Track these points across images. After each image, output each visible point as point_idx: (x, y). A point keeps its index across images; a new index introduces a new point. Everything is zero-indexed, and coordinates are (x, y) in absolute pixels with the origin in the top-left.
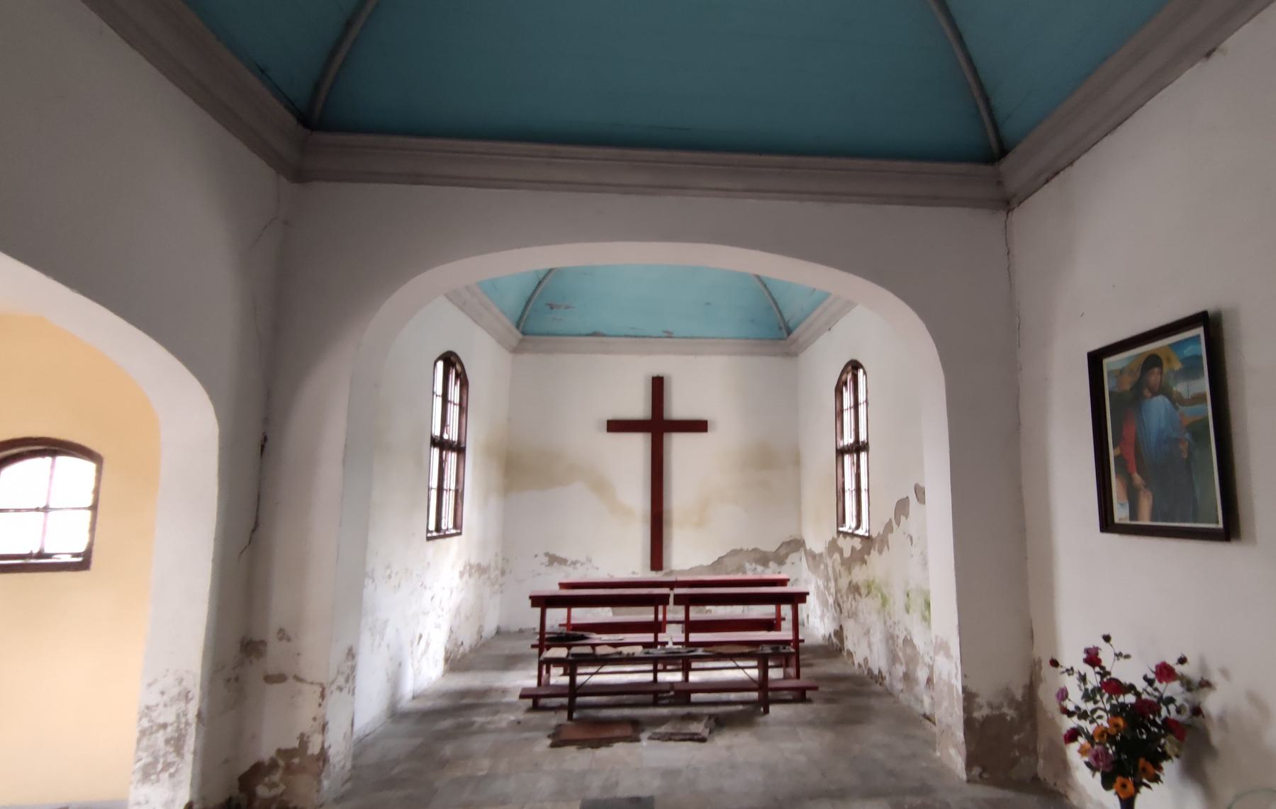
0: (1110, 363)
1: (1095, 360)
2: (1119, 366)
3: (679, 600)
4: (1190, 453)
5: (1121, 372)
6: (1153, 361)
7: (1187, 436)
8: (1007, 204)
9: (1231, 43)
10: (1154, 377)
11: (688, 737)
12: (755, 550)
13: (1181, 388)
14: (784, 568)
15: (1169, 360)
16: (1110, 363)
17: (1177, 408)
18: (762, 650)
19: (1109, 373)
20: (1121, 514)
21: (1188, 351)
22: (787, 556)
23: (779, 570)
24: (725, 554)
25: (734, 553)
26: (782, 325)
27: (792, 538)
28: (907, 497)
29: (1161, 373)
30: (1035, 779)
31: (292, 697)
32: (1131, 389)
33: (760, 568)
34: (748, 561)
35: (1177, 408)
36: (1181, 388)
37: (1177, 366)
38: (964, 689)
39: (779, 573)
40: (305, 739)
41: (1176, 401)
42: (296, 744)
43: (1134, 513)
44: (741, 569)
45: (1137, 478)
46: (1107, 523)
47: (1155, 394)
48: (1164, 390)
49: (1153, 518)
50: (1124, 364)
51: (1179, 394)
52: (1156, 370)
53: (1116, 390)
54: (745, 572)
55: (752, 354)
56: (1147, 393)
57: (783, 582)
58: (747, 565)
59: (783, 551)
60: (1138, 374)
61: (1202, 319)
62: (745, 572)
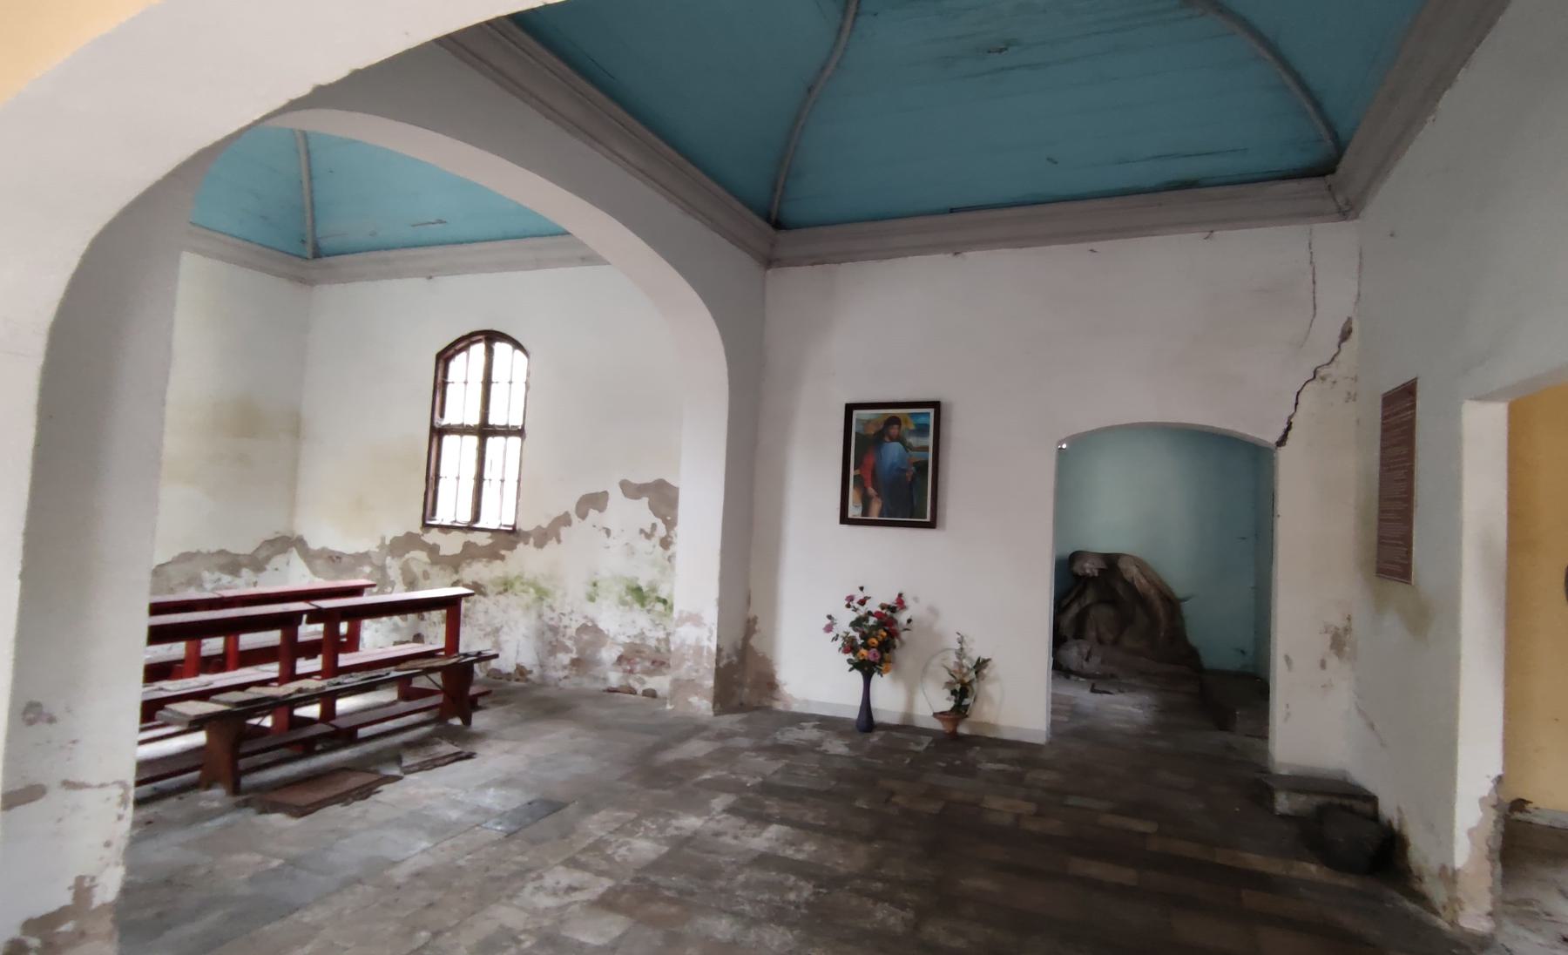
0: (856, 413)
1: (850, 408)
2: (867, 418)
3: (315, 616)
4: (913, 479)
5: (869, 422)
6: (894, 420)
7: (913, 468)
8: (769, 262)
9: (971, 255)
10: (894, 430)
11: (454, 758)
12: (222, 552)
13: (913, 441)
14: (264, 576)
15: (906, 422)
16: (856, 413)
17: (907, 451)
18: (695, 620)
19: (857, 420)
20: (854, 511)
21: (922, 420)
22: (268, 559)
23: (254, 580)
24: (170, 559)
25: (187, 557)
26: (310, 241)
27: (278, 536)
28: (606, 493)
29: (899, 428)
30: (742, 704)
31: (60, 820)
32: (874, 435)
33: (226, 579)
34: (208, 570)
35: (907, 451)
36: (913, 441)
37: (912, 427)
38: (718, 646)
39: (255, 584)
40: (87, 884)
41: (907, 447)
42: (66, 899)
43: (865, 511)
44: (195, 581)
45: (871, 491)
46: (845, 519)
47: (892, 440)
48: (900, 439)
49: (863, 516)
50: (873, 417)
51: (910, 444)
52: (896, 426)
53: (862, 432)
54: (200, 586)
55: (245, 264)
56: (887, 439)
57: (356, 591)
58: (206, 575)
59: (263, 554)
60: (881, 427)
61: (936, 405)
62: (200, 586)
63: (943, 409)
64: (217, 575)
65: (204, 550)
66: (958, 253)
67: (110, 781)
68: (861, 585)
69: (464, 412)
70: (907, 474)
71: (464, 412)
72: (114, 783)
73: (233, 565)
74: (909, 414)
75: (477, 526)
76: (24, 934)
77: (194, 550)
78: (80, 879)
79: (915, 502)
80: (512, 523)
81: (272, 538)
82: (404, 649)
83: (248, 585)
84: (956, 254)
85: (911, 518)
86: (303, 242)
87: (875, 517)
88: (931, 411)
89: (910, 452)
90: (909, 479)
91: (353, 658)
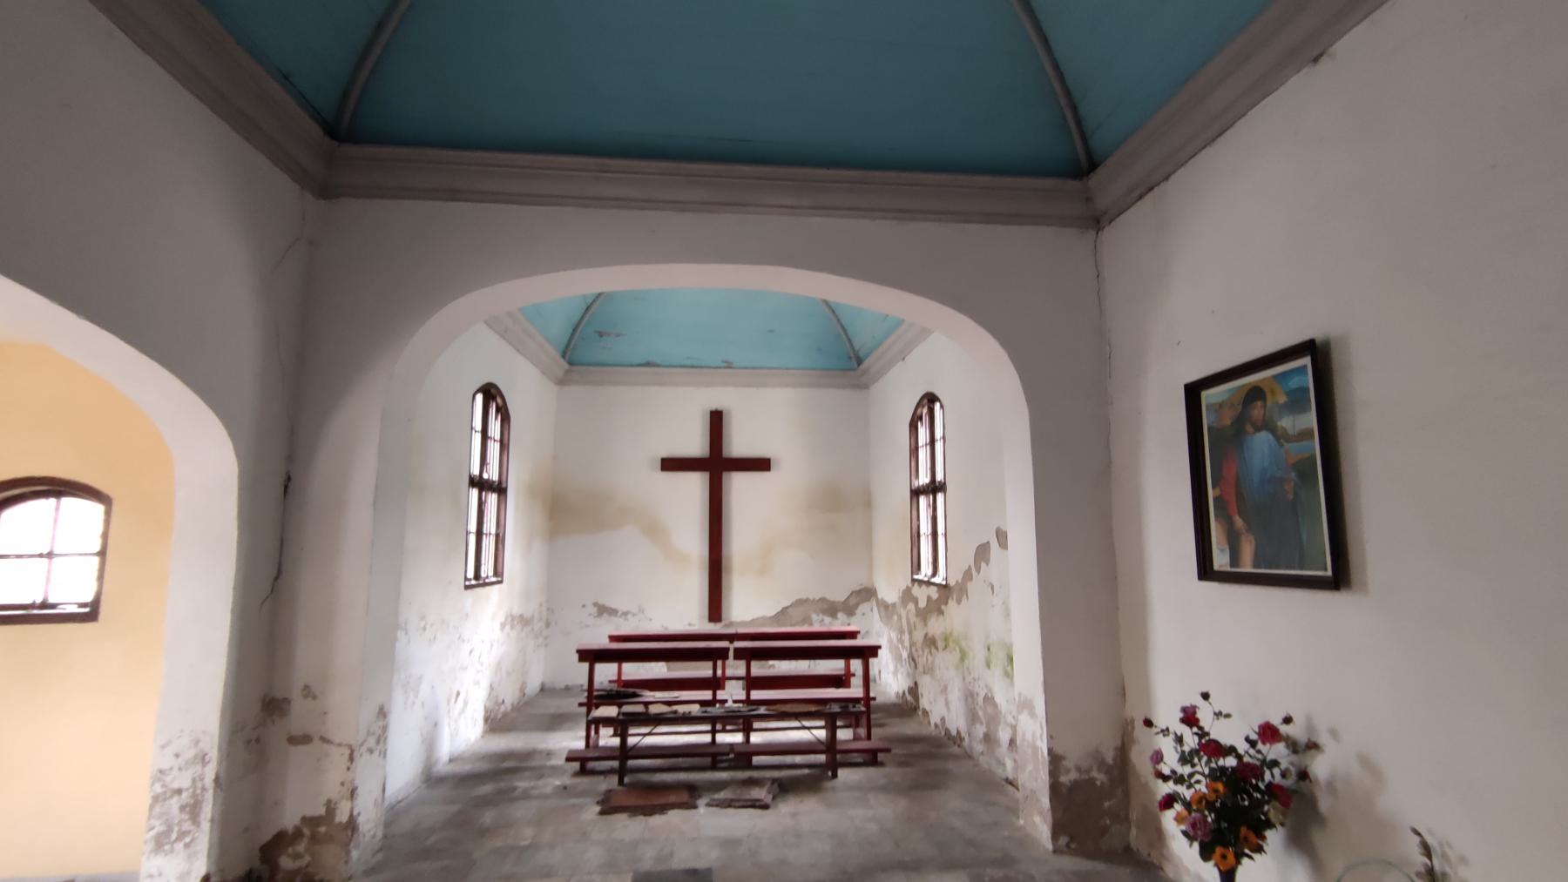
1: (1193, 392)
3: (740, 654)
4: (1296, 494)
6: (1256, 393)
8: (1097, 222)
9: (1340, 46)
10: (1257, 411)
11: (749, 803)
12: (822, 600)
13: (1286, 423)
14: (854, 619)
15: (1273, 393)
16: (1209, 396)
18: (830, 708)
20: (1221, 560)
21: (1294, 383)
22: (857, 606)
23: (848, 622)
24: (789, 604)
25: (800, 602)
26: (852, 355)
29: (1265, 406)
30: (1128, 849)
32: (1232, 424)
33: (827, 620)
34: (815, 612)
35: (1282, 446)
36: (1286, 423)
37: (1282, 399)
38: (1050, 751)
39: (849, 625)
40: (332, 806)
41: (1280, 437)
42: (322, 811)
45: (1239, 522)
46: (1206, 571)
47: (1258, 429)
48: (1268, 425)
50: (1225, 397)
51: (1284, 430)
52: (1259, 403)
54: (811, 624)
55: (818, 386)
56: (1249, 428)
58: (814, 617)
59: (853, 601)
62: (811, 624)
63: (1337, 358)
64: (821, 616)
65: (811, 598)
66: (1321, 55)
67: (345, 742)
68: (1205, 690)
69: (55, 529)
70: (1286, 487)
71: (55, 529)
72: (346, 745)
73: (831, 609)
74: (1275, 377)
75: (933, 580)
76: (302, 823)
77: (804, 597)
78: (329, 801)
79: (1304, 537)
80: (89, 598)
81: (858, 589)
82: (828, 693)
83: (843, 624)
84: (1316, 60)
85: (1301, 569)
86: (850, 358)
87: (1247, 568)
88: (1306, 361)
89: (1285, 444)
90: (1291, 497)
91: (822, 693)
